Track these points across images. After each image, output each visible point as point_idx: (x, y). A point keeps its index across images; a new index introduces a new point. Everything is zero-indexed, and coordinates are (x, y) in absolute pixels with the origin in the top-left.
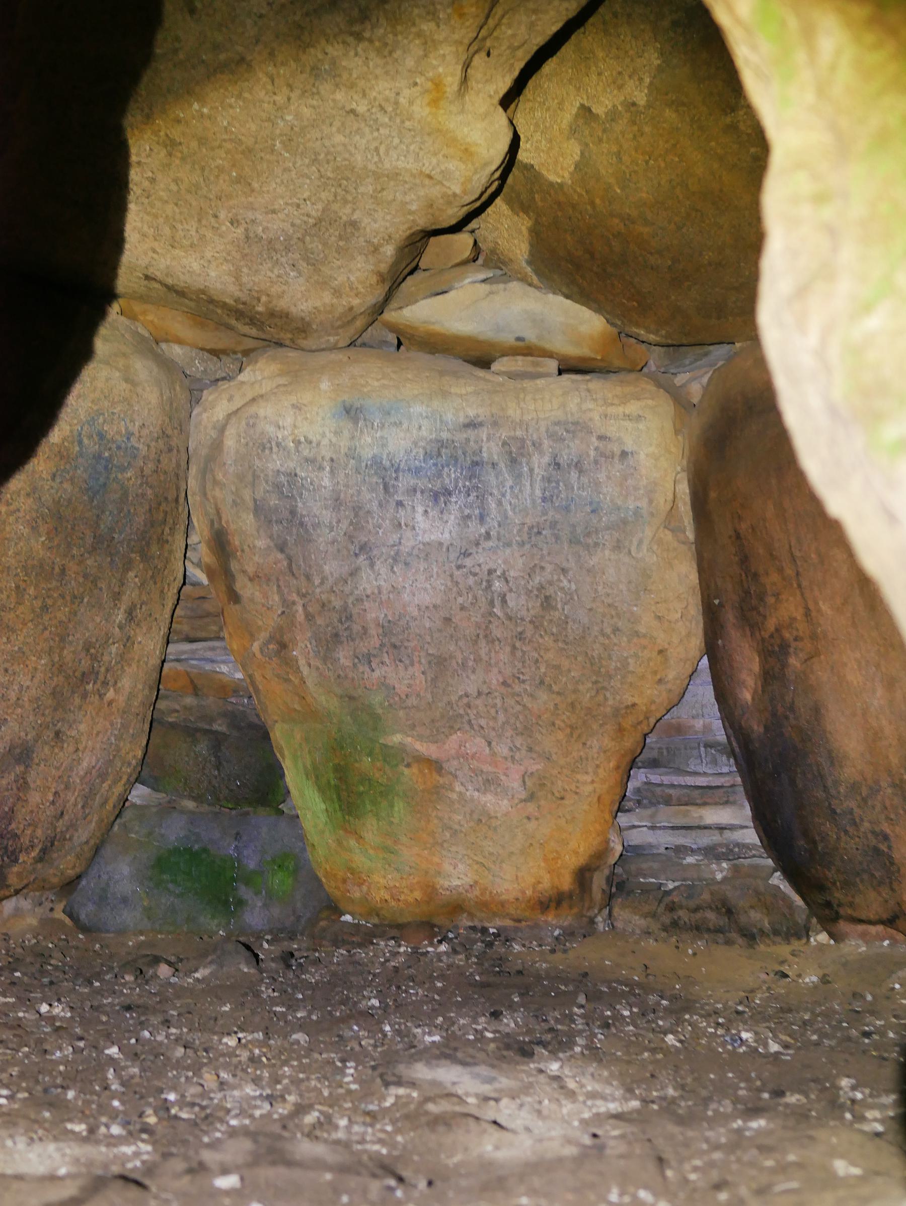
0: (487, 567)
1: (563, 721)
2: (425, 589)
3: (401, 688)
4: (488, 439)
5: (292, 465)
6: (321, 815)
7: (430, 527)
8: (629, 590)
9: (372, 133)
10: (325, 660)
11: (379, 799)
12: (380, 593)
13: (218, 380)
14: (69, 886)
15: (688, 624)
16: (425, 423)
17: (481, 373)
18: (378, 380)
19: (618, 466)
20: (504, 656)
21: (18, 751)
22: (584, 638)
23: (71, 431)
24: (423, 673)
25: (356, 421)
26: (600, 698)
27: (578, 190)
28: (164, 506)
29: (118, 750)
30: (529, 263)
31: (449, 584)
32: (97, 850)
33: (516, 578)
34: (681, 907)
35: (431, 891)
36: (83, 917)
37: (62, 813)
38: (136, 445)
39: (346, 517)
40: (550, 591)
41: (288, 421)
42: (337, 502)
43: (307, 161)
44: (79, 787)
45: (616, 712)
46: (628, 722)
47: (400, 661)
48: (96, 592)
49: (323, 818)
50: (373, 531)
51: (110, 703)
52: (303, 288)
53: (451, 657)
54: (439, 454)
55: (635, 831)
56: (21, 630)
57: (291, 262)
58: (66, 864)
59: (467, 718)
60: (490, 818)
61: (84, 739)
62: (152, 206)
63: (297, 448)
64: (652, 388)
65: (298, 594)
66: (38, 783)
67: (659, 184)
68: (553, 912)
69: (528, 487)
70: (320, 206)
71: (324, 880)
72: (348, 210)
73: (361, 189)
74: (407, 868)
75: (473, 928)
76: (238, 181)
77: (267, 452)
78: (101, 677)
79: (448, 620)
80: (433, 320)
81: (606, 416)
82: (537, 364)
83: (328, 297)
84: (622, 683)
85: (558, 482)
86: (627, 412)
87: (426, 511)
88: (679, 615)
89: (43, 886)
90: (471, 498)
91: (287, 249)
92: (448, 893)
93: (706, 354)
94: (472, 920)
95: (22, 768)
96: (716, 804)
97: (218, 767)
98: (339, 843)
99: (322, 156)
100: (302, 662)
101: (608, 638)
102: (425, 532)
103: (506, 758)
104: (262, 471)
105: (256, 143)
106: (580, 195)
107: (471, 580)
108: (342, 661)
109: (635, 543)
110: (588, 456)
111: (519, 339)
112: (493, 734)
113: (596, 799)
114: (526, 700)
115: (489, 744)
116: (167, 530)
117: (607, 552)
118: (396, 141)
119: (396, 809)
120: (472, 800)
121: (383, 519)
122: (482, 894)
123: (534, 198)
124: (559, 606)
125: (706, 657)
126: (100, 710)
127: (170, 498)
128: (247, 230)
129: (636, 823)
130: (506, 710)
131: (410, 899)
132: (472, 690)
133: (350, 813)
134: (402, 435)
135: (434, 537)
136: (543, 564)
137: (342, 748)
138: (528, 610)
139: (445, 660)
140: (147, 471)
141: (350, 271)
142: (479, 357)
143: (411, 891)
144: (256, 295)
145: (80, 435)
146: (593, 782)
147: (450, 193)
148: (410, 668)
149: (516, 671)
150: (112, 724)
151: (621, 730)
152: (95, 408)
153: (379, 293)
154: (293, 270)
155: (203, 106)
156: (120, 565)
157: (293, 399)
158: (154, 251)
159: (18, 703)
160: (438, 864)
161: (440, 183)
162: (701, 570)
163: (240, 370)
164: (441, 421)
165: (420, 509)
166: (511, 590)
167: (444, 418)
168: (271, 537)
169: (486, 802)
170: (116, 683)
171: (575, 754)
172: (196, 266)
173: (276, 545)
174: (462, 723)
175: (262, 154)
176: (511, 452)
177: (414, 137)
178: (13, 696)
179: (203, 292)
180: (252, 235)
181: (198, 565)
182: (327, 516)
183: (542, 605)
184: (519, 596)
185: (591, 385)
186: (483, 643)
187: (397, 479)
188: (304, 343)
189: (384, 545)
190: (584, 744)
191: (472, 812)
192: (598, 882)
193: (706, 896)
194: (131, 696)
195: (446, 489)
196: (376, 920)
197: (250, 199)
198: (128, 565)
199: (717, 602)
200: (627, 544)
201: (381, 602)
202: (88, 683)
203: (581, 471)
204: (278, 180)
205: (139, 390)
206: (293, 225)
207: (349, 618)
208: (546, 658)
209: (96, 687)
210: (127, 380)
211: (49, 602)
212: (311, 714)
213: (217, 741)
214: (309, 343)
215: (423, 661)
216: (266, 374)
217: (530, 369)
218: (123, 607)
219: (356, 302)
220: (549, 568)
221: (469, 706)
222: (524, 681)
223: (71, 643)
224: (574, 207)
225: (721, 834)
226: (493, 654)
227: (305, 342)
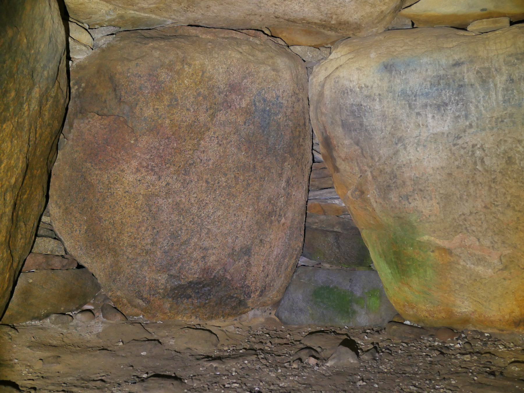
0: (472, 143)
2: (436, 159)
3: (426, 212)
4: (468, 71)
5: (359, 100)
7: (437, 124)
10: (384, 199)
11: (418, 268)
12: (411, 162)
13: (320, 60)
14: (277, 304)
17: (462, 32)
18: (401, 47)
20: (484, 192)
21: (244, 250)
24: (438, 203)
25: (391, 72)
31: (449, 155)
32: (287, 288)
33: (489, 148)
35: (450, 314)
36: (283, 317)
37: (268, 275)
38: (282, 102)
39: (390, 124)
40: (511, 154)
44: (274, 263)
47: (425, 198)
49: (390, 277)
51: (283, 224)
52: (354, 7)
53: (453, 194)
54: (439, 84)
60: (481, 279)
63: (361, 90)
65: (368, 166)
66: (255, 263)
69: (494, 96)
71: (394, 305)
75: (476, 331)
77: (346, 95)
78: (278, 213)
79: (450, 175)
82: (496, 22)
83: (368, 9)
85: (513, 90)
87: (433, 116)
90: (459, 106)
92: (460, 314)
97: (339, 247)
98: (400, 288)
100: (372, 201)
102: (433, 127)
103: (489, 247)
104: (344, 105)
107: (462, 152)
108: (393, 199)
111: (483, 10)
112: (480, 234)
114: (499, 215)
115: (479, 240)
116: (301, 140)
119: (428, 273)
121: (410, 123)
122: (479, 316)
124: (517, 162)
127: (301, 124)
130: (487, 222)
132: (467, 211)
133: (404, 275)
134: (417, 76)
135: (439, 130)
136: (506, 139)
137: (397, 243)
138: (498, 166)
139: (450, 196)
144: (330, 16)
145: (254, 101)
149: (492, 200)
150: (285, 234)
152: (260, 87)
156: (280, 160)
157: (357, 65)
159: (242, 229)
164: (439, 65)
165: (430, 115)
166: (486, 155)
167: (441, 63)
168: (351, 138)
170: (285, 215)
172: (297, 7)
174: (462, 229)
176: (482, 77)
178: (239, 226)
179: (304, 19)
182: (379, 125)
183: (506, 162)
184: (492, 158)
186: (471, 186)
187: (415, 100)
188: (360, 34)
189: (411, 137)
191: (471, 276)
194: (293, 220)
198: (284, 160)
201: (412, 168)
205: (280, 74)
209: (276, 218)
210: (274, 70)
211: (250, 182)
213: (337, 235)
214: (363, 34)
215: (437, 197)
217: (492, 26)
218: (284, 180)
219: (384, 8)
220: (510, 140)
221: (465, 220)
222: (497, 206)
226: (478, 191)
227: (360, 34)
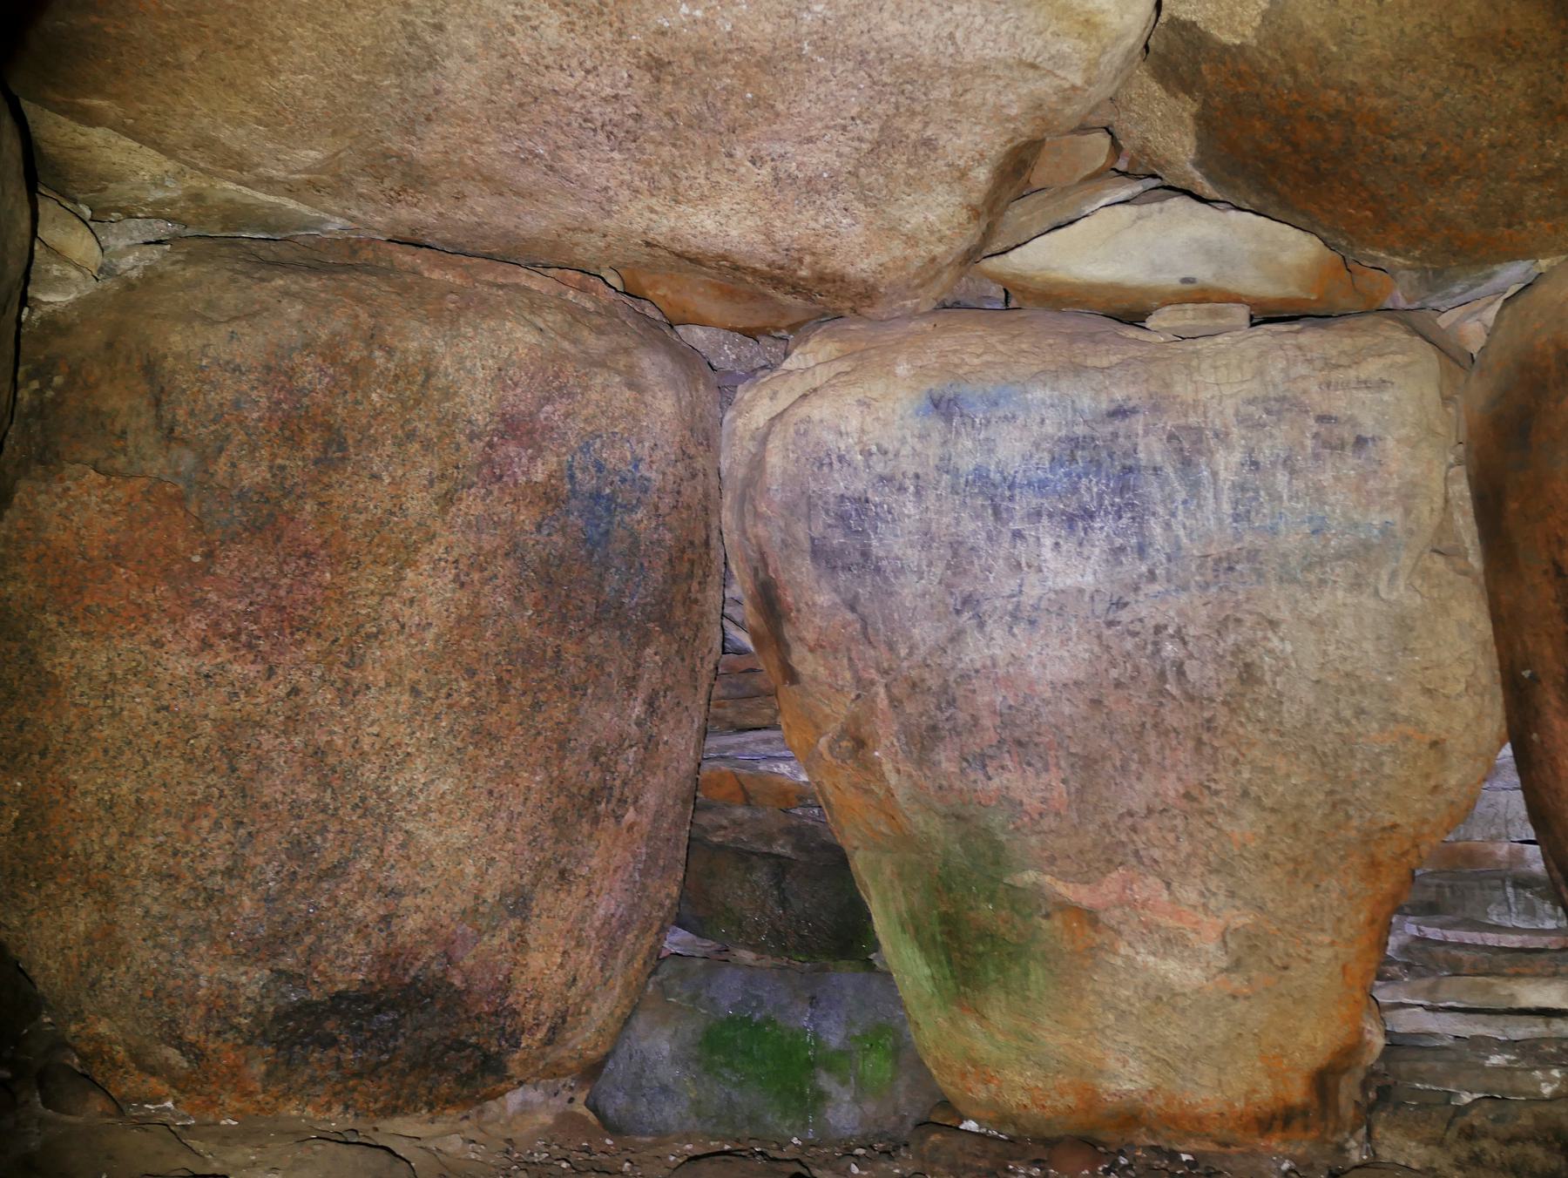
0: (1153, 623)
1: (1282, 852)
2: (1061, 658)
4: (1146, 433)
6: (924, 983)
7: (1067, 568)
8: (1378, 651)
9: (942, 13)
10: (920, 763)
12: (994, 665)
14: (592, 1071)
15: (1477, 698)
16: (1050, 414)
17: (1132, 333)
18: (978, 356)
19: (1352, 460)
22: (1309, 725)
23: (559, 464)
24: (1064, 781)
25: (948, 418)
26: (1340, 816)
27: (1269, 53)
28: (689, 554)
29: (644, 888)
30: (1197, 164)
31: (1097, 649)
33: (1198, 638)
34: (1485, 1135)
35: (1090, 1098)
36: (610, 1112)
37: (575, 979)
38: (647, 474)
39: (941, 558)
40: (1252, 655)
41: (854, 424)
42: (927, 537)
43: (850, 65)
44: (595, 943)
45: (1366, 838)
46: (1385, 852)
47: (1029, 764)
48: (603, 679)
49: (928, 986)
50: (980, 575)
51: (630, 828)
52: (862, 239)
53: (1104, 758)
54: (1073, 459)
55: (1404, 1012)
56: (507, 737)
57: (842, 205)
58: (583, 1039)
59: (1131, 847)
61: (598, 878)
62: (642, 151)
64: (1401, 335)
65: (878, 670)
67: (1402, 31)
68: (1279, 1134)
69: (1211, 501)
70: (876, 125)
71: (934, 1072)
72: (917, 124)
73: (935, 94)
74: (1053, 1063)
76: (754, 104)
77: (826, 469)
78: (616, 793)
79: (1096, 703)
80: (1054, 265)
81: (1328, 385)
83: (898, 248)
84: (1374, 793)
85: (1256, 490)
86: (1363, 377)
87: (1057, 544)
88: (1463, 686)
89: (555, 1071)
90: (1124, 521)
91: (835, 188)
92: (1116, 1099)
93: (1488, 277)
94: (1154, 1138)
95: (519, 923)
96: (1537, 975)
99: (873, 54)
100: (888, 767)
101: (1348, 724)
102: (1056, 574)
103: (1195, 907)
104: (820, 497)
105: (775, 49)
106: (1273, 61)
107: (1129, 644)
108: (944, 765)
109: (1385, 576)
110: (1303, 447)
111: (1185, 281)
112: (1173, 870)
113: (1338, 969)
115: (1168, 885)
116: (695, 586)
117: (1340, 594)
118: (979, 20)
119: (1033, 978)
120: (1146, 968)
123: (1199, 71)
124: (1268, 677)
125: (1508, 745)
126: (616, 838)
128: (774, 169)
129: (1406, 1001)
130: (1191, 835)
131: (1060, 1105)
132: (1138, 805)
133: (965, 984)
134: (1017, 434)
135: (1069, 581)
136: (1238, 615)
137: (950, 889)
138: (1219, 685)
139: (1096, 762)
140: (663, 509)
141: (928, 208)
142: (1128, 311)
143: (1062, 1095)
144: (796, 255)
146: (1333, 943)
147: (1067, 85)
148: (1044, 775)
149: (1203, 777)
150: (634, 856)
151: (1374, 864)
153: (973, 233)
154: (845, 217)
155: (695, 8)
156: (634, 640)
157: (858, 392)
158: (652, 211)
160: (1099, 1060)
161: (1051, 73)
162: (1496, 619)
163: (787, 355)
164: (1075, 410)
165: (1048, 542)
166: (1191, 656)
167: (1078, 405)
168: (836, 590)
169: (1167, 972)
170: (636, 801)
171: (1303, 902)
172: (710, 225)
173: (844, 601)
174: (1126, 855)
175: (786, 64)
177: (1006, 11)
179: (724, 258)
180: (782, 175)
181: (740, 625)
182: (913, 556)
183: (1240, 676)
184: (1204, 664)
185: (1304, 339)
186: (1151, 736)
187: (1012, 498)
189: (997, 595)
190: (1317, 886)
192: (1348, 1091)
193: (1526, 1121)
194: (659, 815)
195: (1085, 510)
196: (1012, 1131)
197: (775, 127)
198: (645, 639)
199: (1526, 674)
200: (1371, 580)
202: (599, 803)
203: (1293, 472)
204: (812, 96)
205: (648, 398)
206: (839, 155)
207: (952, 702)
208: (1249, 757)
209: (611, 806)
210: (631, 385)
211: (542, 697)
212: (905, 840)
213: (780, 866)
214: (879, 310)
215: (1063, 763)
216: (821, 358)
218: (641, 697)
219: (939, 249)
221: (1134, 829)
223: (574, 750)
224: (1263, 78)
225: (1547, 1025)
226: (1168, 752)
227: (871, 311)
